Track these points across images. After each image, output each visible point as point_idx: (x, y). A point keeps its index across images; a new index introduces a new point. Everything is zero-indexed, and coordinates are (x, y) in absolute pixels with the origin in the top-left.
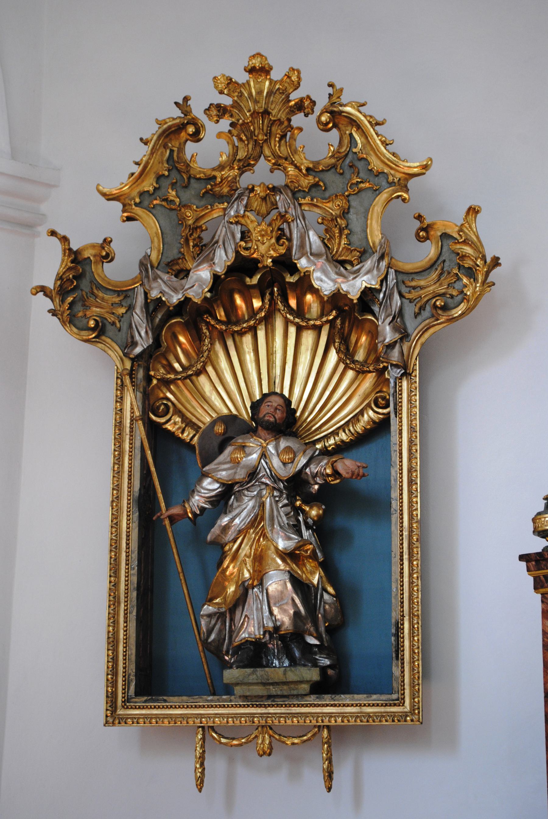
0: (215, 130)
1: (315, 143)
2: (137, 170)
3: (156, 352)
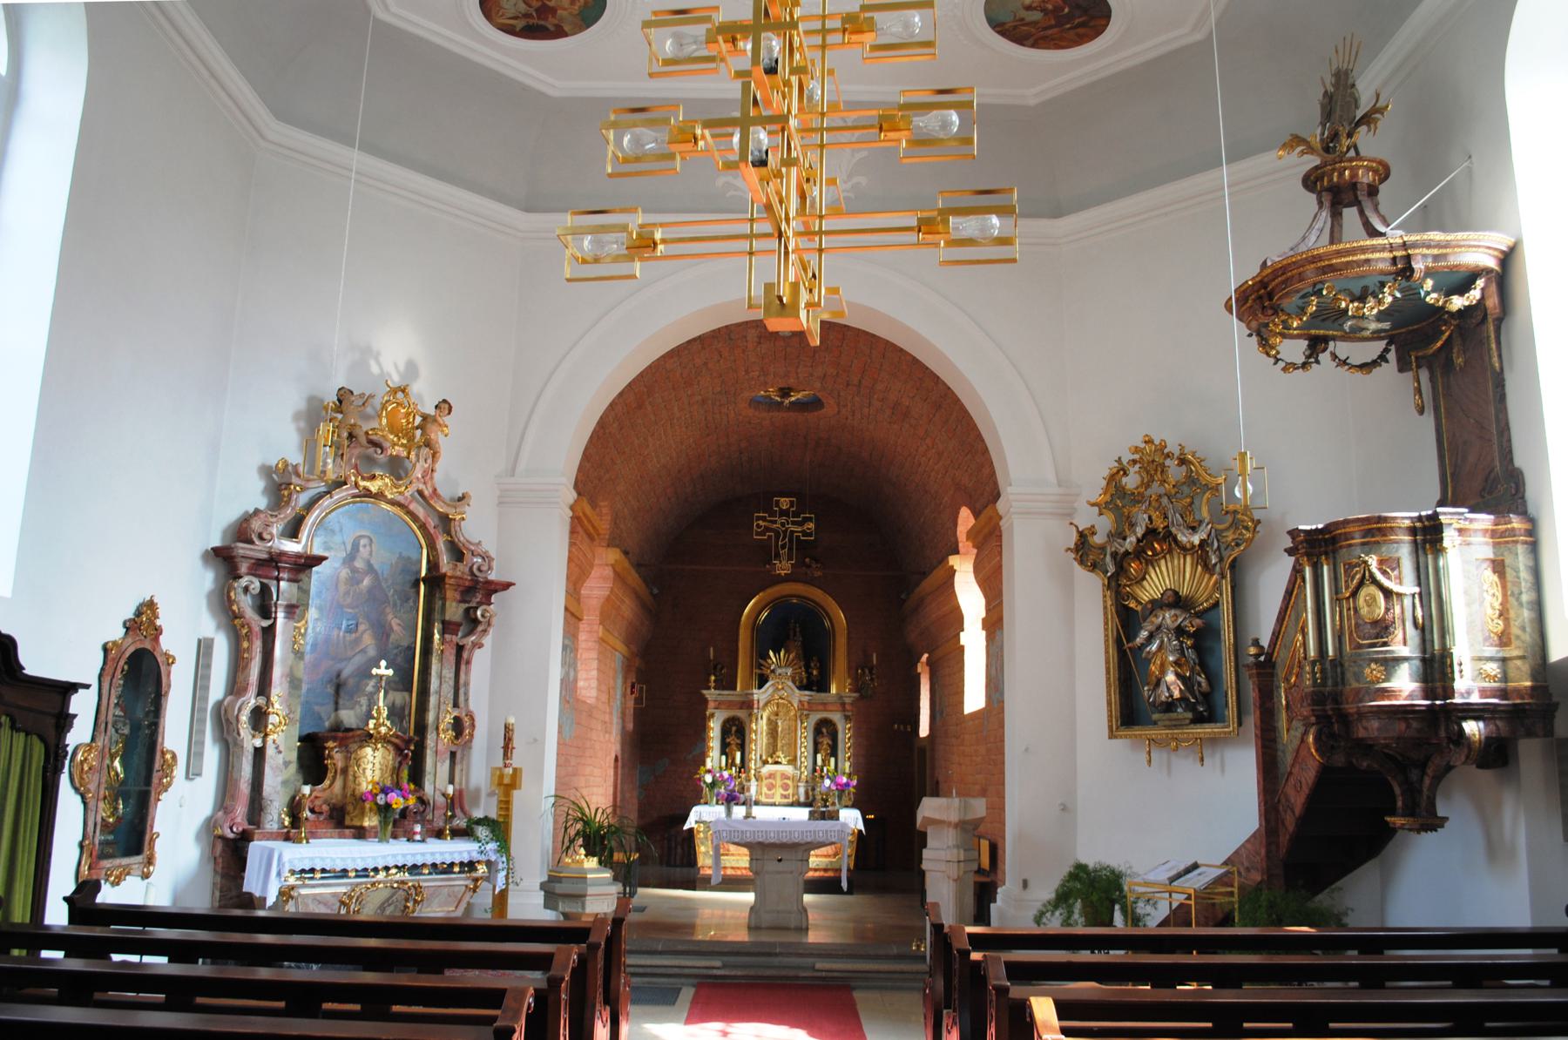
0: (1133, 470)
1: (1175, 472)
2: (1254, 338)
3: (1121, 569)
